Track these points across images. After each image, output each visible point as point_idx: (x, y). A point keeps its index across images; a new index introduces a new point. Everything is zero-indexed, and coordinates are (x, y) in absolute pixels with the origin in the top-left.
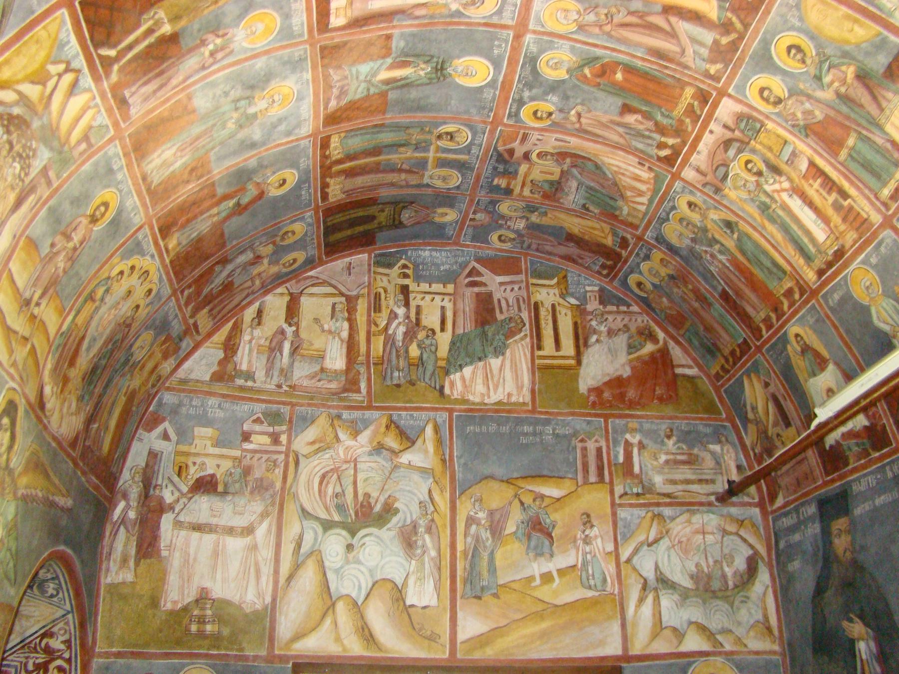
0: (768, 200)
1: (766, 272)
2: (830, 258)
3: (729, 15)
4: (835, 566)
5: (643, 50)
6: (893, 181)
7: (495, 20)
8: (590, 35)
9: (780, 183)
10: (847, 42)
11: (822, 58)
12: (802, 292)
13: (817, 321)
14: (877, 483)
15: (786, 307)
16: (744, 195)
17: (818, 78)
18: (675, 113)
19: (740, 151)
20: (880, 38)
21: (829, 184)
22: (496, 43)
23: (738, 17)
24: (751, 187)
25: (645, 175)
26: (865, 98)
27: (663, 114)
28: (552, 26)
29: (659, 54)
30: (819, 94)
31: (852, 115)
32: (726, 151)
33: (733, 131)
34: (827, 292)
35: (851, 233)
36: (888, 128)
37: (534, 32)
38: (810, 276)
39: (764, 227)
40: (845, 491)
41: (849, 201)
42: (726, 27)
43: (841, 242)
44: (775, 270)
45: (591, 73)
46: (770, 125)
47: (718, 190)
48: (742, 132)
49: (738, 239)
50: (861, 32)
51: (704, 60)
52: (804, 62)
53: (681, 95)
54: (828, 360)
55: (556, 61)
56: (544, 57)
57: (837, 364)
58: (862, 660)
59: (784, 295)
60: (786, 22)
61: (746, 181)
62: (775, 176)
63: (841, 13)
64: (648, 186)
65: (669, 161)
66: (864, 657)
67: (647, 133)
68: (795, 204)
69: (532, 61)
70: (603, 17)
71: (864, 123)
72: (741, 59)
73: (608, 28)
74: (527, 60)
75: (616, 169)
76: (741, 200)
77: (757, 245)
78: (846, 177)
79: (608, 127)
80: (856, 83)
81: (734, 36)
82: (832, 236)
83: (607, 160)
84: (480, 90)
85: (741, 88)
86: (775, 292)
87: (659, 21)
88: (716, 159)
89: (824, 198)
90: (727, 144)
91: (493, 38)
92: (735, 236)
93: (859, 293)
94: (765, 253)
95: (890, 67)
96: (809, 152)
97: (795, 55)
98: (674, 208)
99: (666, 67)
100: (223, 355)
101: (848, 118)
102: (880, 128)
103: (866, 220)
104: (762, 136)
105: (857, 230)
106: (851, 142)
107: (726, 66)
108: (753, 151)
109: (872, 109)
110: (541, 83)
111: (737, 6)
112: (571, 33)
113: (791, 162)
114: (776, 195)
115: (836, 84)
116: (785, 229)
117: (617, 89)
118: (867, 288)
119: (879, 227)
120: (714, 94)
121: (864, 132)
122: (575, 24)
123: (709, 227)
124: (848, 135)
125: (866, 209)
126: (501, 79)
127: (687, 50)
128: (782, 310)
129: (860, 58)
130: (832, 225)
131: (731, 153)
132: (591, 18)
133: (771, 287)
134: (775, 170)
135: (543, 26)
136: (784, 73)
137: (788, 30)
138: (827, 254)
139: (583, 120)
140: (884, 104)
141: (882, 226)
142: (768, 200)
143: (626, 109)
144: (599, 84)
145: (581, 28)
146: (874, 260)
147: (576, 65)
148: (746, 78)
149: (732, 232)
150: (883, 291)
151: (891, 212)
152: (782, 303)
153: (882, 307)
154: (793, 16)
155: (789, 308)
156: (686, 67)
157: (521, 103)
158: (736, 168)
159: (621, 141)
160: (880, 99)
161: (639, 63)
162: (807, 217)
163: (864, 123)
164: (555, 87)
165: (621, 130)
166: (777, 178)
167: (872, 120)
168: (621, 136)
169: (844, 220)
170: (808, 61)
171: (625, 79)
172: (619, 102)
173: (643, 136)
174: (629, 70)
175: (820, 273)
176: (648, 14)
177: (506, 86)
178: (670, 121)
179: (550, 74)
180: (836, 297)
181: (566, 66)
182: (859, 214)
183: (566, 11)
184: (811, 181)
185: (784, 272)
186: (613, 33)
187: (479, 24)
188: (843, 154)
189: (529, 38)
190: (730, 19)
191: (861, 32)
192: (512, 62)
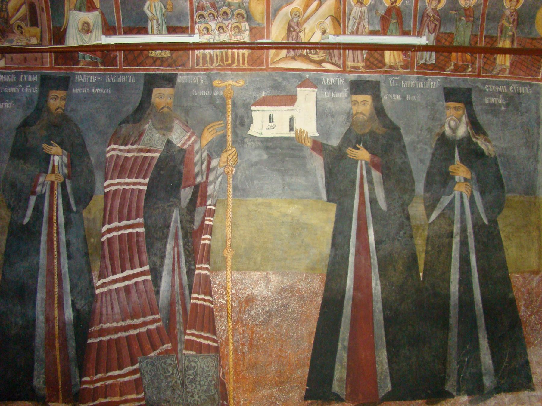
4: (45, 115)
14: (96, 81)
40: (69, 78)
58: (54, 166)
66: (56, 164)
100: (156, 92)
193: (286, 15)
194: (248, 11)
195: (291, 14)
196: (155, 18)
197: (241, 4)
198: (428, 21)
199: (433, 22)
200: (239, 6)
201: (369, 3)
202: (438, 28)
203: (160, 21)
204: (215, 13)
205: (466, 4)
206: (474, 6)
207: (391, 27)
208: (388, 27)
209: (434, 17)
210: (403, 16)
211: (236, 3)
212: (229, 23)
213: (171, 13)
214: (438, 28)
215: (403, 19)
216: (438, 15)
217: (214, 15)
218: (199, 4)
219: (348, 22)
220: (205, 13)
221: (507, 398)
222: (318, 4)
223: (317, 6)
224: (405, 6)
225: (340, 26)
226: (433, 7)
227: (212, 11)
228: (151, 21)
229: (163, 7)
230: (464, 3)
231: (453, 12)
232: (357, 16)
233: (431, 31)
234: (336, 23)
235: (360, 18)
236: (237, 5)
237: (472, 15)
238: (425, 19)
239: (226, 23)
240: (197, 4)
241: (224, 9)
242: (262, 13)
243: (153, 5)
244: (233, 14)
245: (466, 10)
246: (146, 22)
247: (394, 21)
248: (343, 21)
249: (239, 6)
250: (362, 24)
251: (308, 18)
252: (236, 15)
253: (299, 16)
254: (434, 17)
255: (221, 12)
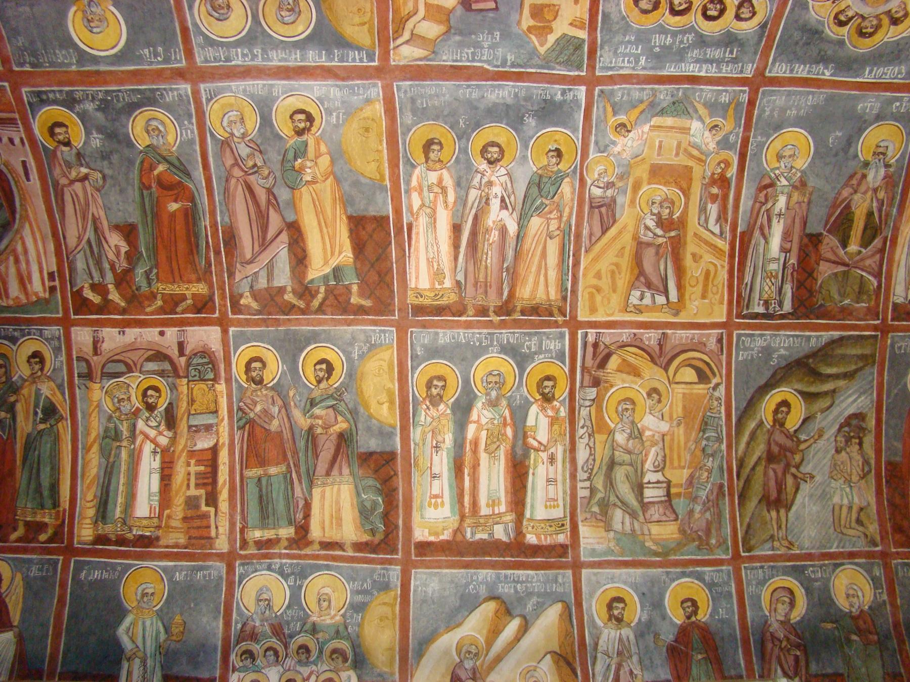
0: (126, 433)
1: (33, 486)
2: (129, 536)
3: (322, 289)
5: (227, 219)
6: (273, 532)
7: (196, 40)
8: (220, 156)
9: (161, 433)
10: (367, 407)
11: (337, 395)
12: (57, 536)
13: (43, 579)
15: (14, 536)
16: (108, 406)
17: (313, 403)
18: (161, 286)
19: (162, 374)
20: (390, 430)
21: (209, 479)
22: (160, 49)
23: (325, 299)
24: (126, 407)
25: (37, 286)
26: (326, 455)
27: (147, 274)
28: (213, 112)
29: (231, 239)
30: (297, 414)
31: (301, 455)
32: (148, 359)
33: (181, 353)
34: (89, 562)
35: (181, 535)
36: (316, 492)
37: (196, 93)
38: (85, 532)
39: (87, 450)
41: (212, 510)
42: (306, 291)
43: (160, 533)
44: (46, 493)
45: (161, 173)
46: (221, 387)
47: (89, 376)
48: (188, 364)
49: (41, 433)
50: (384, 412)
51: (251, 287)
52: (319, 382)
53: (189, 282)
54: (12, 626)
55: (161, 128)
56: (159, 113)
57: (21, 640)
59: (27, 524)
60: (351, 344)
61: (129, 399)
62: (163, 423)
63: (390, 385)
64: (23, 297)
65: (82, 305)
67: (107, 266)
68: (149, 464)
69: (150, 100)
70: (251, 163)
71: (303, 469)
72: (277, 323)
73: (237, 173)
74: (148, 94)
75: (20, 248)
76: (98, 406)
77: (55, 456)
78: (232, 490)
79: (84, 218)
80: (334, 438)
81: (302, 304)
82: (156, 520)
83: (27, 232)
84: (67, 43)
85: (243, 338)
86: (19, 512)
87: (275, 222)
88: (129, 354)
89: (188, 485)
90: (159, 356)
91: (168, 41)
92: (42, 426)
93: (129, 593)
94: (56, 470)
95: (371, 454)
96: (224, 438)
97: (321, 370)
98: (14, 340)
99: (217, 253)
101: (295, 453)
102: (311, 484)
103: (210, 538)
104: (199, 389)
105: (190, 538)
106: (273, 470)
107: (259, 312)
108: (173, 388)
109: (322, 466)
110: (114, 120)
111: (336, 292)
112: (212, 135)
113: (195, 430)
114: (140, 439)
115: (320, 422)
116: (109, 471)
117: (156, 213)
118: (144, 595)
119: (218, 555)
120: (217, 315)
121: (294, 475)
122: (227, 135)
123: (25, 391)
124: (277, 464)
125: (221, 530)
126: (103, 68)
127: (252, 265)
128: (8, 535)
129: (360, 426)
130: (167, 512)
131: (151, 366)
132: (244, 151)
133: (20, 503)
134: (170, 420)
135: (208, 100)
136: (294, 369)
137: (344, 351)
138: (131, 530)
139: (78, 186)
140: (335, 472)
141: (220, 556)
142: (126, 433)
143: (128, 232)
144: (149, 188)
145: (225, 144)
146: (178, 577)
147: (165, 153)
148: (260, 338)
149: (43, 421)
150: (161, 609)
151: (242, 552)
152: (15, 529)
153: (144, 623)
154: (360, 348)
155: (19, 540)
156: (231, 275)
157: (70, 102)
158: (135, 382)
159: (72, 241)
160: (337, 466)
161: (206, 222)
162: (148, 482)
163: (303, 469)
164: (117, 138)
165: (90, 233)
166: (163, 427)
167: (311, 473)
168: (80, 239)
169: (185, 519)
170: (323, 385)
171: (173, 215)
172: (134, 216)
173: (98, 263)
174: (190, 216)
175: (101, 539)
176: (278, 209)
177: (98, 77)
178: (144, 284)
179: (138, 129)
180: (96, 574)
181: (158, 141)
182: (209, 527)
183: (242, 120)
184: (193, 462)
185: (56, 504)
186: (233, 181)
187: (183, 22)
188: (253, 473)
189: (186, 88)
190: (317, 292)
191: (384, 412)
192: (137, 76)
193: (447, 652)
194: (356, 646)
195: (459, 654)
196: (140, 654)
197: (341, 629)
198: (776, 650)
199: (788, 650)
200: (337, 632)
201: (636, 620)
202: (802, 663)
203: (149, 662)
204: (280, 648)
205: (851, 605)
206: (870, 608)
207: (694, 671)
208: (688, 670)
209: (788, 639)
210: (718, 643)
211: (329, 626)
212: (311, 673)
213: (178, 646)
214: (802, 663)
215: (720, 651)
216: (797, 635)
217: (276, 653)
218: (244, 625)
219: (594, 664)
220: (256, 648)
221: (539, 2)
222: (520, 627)
223: (519, 631)
224: (719, 620)
225: (576, 676)
226: (782, 619)
227: (274, 642)
228: (129, 660)
229: (162, 630)
230: (847, 605)
231: (829, 626)
232: (613, 651)
233: (790, 674)
234: (566, 670)
235: (619, 653)
236: (332, 631)
237: (872, 629)
238: (769, 646)
239: (305, 671)
240: (239, 626)
241: (301, 639)
242: (391, 649)
243: (140, 623)
244: (321, 652)
245: (854, 618)
246: (118, 662)
247: (700, 657)
248: (581, 664)
249: (337, 632)
250: (627, 669)
251: (499, 659)
252: (328, 654)
253: (476, 655)
254: (788, 639)
255: (293, 646)
